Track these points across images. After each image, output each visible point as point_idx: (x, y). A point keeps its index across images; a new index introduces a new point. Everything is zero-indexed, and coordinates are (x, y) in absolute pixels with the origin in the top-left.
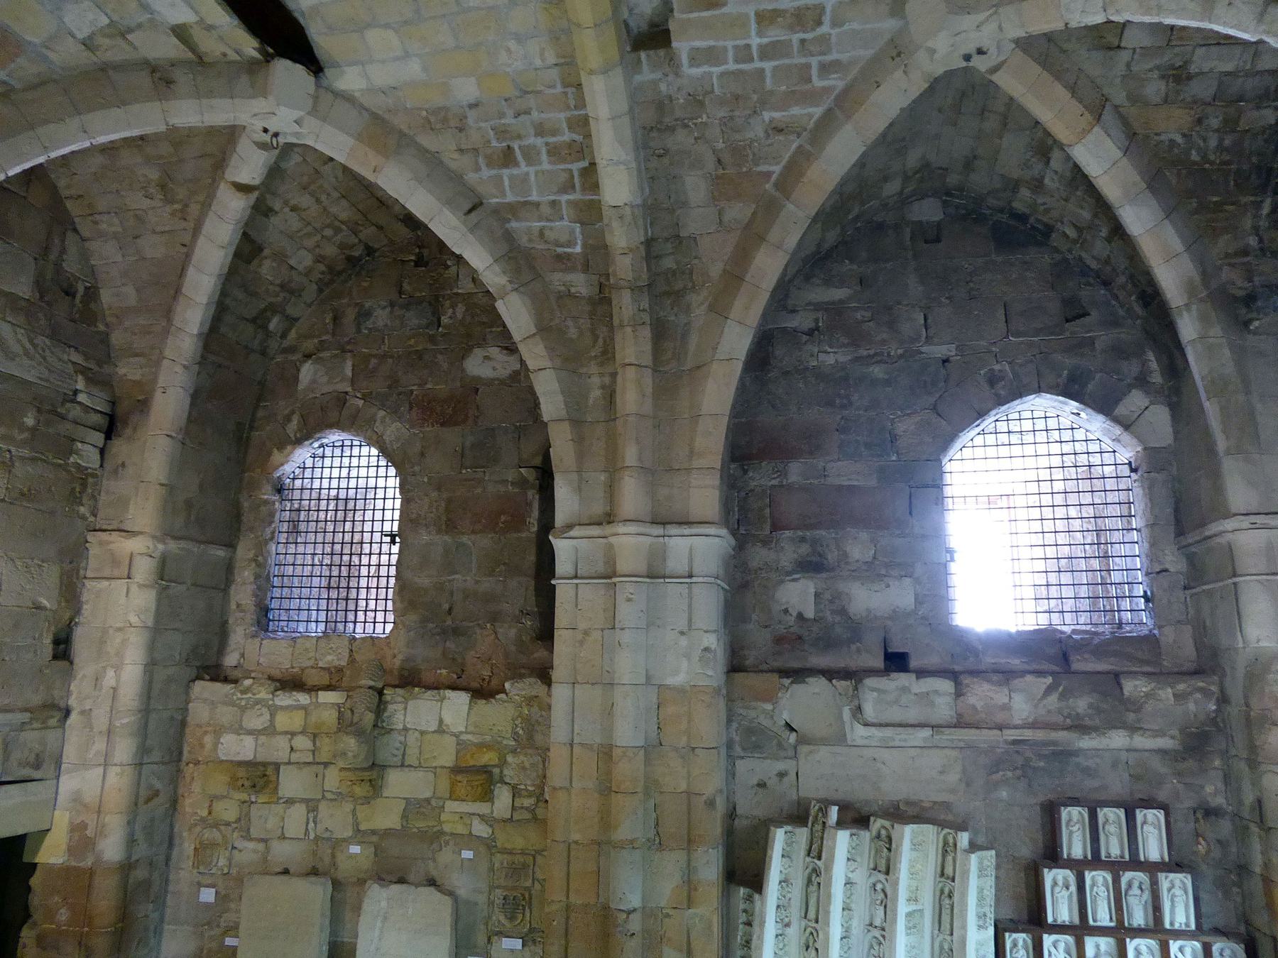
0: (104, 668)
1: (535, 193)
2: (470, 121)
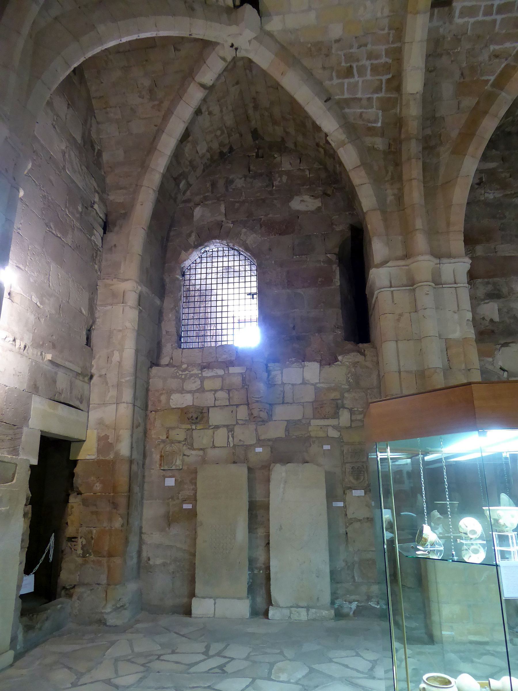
0: (113, 351)
1: (360, 93)
2: (333, 51)
